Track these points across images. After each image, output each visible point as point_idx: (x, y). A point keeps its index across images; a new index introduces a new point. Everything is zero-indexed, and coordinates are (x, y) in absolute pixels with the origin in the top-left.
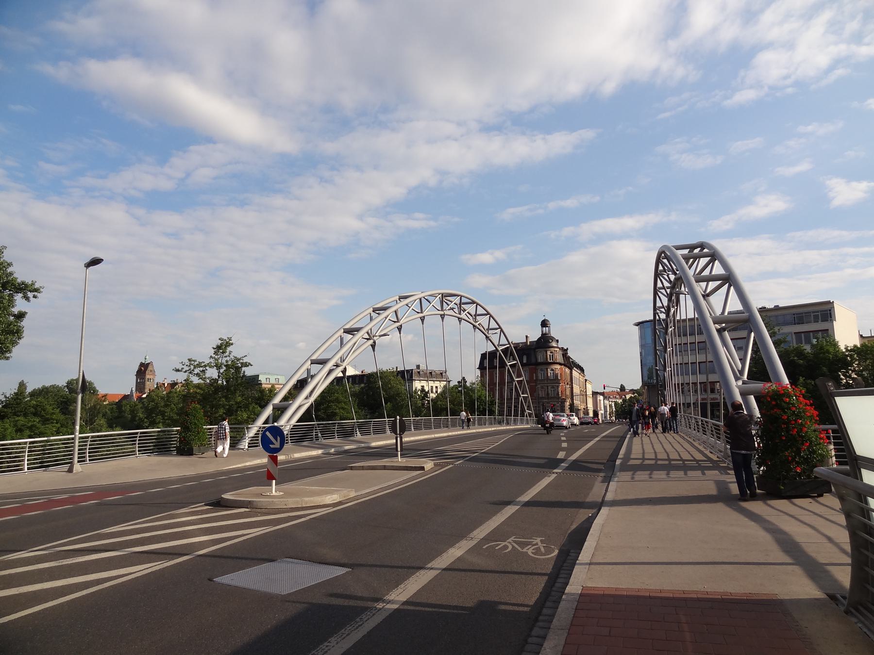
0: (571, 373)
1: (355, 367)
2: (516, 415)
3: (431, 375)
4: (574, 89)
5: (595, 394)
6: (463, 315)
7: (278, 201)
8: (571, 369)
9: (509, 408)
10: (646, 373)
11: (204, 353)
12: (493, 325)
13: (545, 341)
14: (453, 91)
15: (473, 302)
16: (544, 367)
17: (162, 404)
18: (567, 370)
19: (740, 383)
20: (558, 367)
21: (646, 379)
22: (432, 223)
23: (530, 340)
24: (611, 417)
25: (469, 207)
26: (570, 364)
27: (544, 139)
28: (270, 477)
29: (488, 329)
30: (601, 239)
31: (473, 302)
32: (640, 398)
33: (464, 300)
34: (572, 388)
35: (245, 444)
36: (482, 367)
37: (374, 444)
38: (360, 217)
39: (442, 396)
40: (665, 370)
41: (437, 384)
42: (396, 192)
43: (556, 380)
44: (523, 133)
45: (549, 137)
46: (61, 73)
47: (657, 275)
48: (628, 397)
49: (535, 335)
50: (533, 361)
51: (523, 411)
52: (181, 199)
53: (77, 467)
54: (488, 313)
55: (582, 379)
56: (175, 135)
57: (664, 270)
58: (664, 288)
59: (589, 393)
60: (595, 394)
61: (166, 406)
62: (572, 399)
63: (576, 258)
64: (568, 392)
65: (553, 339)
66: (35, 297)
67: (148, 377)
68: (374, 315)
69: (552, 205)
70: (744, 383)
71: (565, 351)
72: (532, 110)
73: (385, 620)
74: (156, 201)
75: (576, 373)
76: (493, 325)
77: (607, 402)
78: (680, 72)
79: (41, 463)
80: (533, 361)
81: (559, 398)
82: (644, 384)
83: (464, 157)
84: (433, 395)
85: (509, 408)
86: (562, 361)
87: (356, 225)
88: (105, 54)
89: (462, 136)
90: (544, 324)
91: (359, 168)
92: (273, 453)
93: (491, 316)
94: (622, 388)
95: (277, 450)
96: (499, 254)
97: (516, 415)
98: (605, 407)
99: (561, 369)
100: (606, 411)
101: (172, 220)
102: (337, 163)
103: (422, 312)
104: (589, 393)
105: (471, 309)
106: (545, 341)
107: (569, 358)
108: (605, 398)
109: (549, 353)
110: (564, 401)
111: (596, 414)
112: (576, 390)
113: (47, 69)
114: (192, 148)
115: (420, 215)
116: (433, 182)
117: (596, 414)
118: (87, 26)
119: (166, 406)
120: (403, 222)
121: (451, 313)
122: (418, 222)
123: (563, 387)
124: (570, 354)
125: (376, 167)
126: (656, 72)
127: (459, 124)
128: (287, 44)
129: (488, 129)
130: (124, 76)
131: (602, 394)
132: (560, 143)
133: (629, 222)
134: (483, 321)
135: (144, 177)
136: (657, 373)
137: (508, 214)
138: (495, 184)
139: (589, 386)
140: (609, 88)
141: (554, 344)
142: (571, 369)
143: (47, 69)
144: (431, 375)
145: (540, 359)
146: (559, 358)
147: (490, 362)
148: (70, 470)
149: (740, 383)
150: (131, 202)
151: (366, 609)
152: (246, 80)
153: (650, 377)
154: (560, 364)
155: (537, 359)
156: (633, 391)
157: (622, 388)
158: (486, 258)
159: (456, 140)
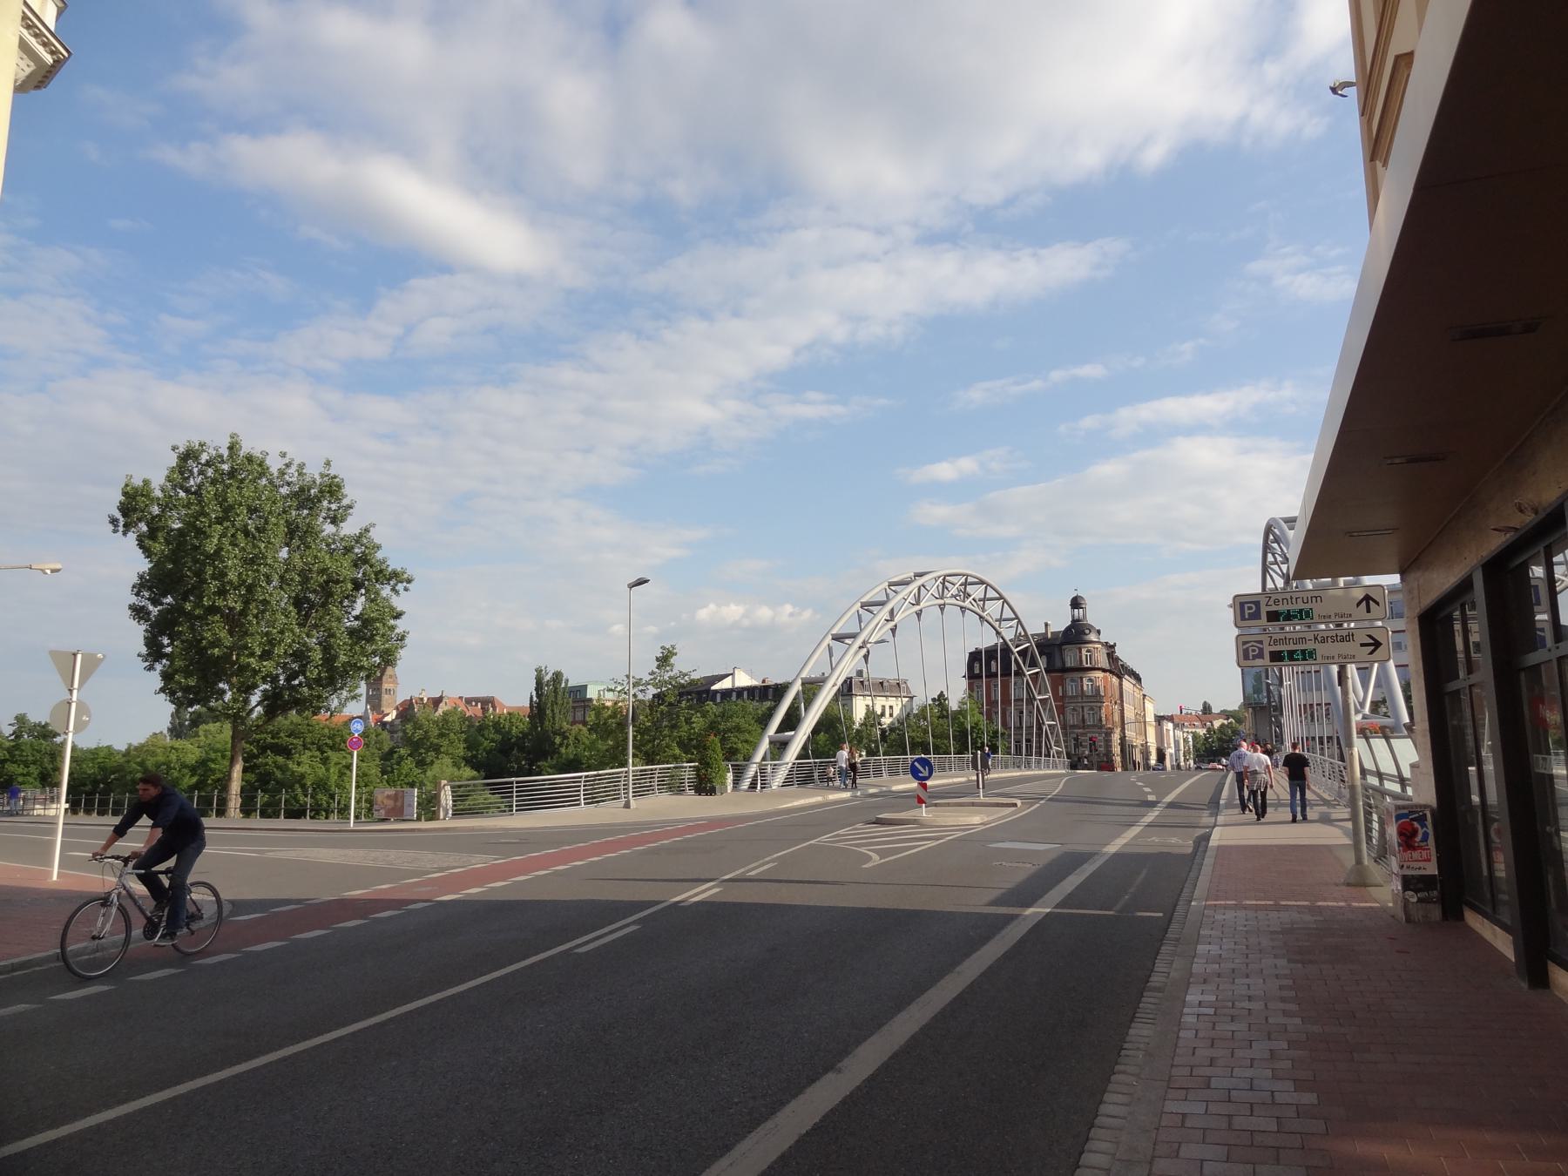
0: (1121, 685)
1: (751, 674)
2: (1029, 753)
3: (882, 687)
4: (1088, 159)
5: (1160, 719)
6: (967, 604)
7: (566, 374)
8: (1120, 677)
9: (1018, 742)
10: (1250, 682)
11: (644, 667)
12: (1008, 613)
13: (1076, 633)
14: (863, 167)
15: (982, 582)
16: (1076, 675)
17: (436, 732)
18: (1115, 680)
19: (1359, 717)
20: (1100, 674)
21: (1250, 690)
22: (839, 409)
23: (1052, 629)
24: (1186, 760)
25: (911, 384)
26: (1118, 669)
27: (1035, 255)
28: (921, 801)
29: (1000, 620)
30: (1154, 435)
31: (982, 582)
32: (1241, 728)
33: (970, 579)
34: (1122, 711)
35: (746, 784)
36: (972, 676)
37: (894, 788)
38: (711, 400)
39: (906, 719)
40: (1281, 684)
41: (892, 701)
42: (776, 355)
43: (1097, 697)
44: (997, 247)
45: (1043, 252)
46: (191, 160)
47: (1265, 570)
48: (1217, 724)
49: (1060, 623)
50: (1058, 664)
51: (1048, 749)
52: (399, 375)
53: (633, 803)
54: (1001, 597)
55: (1138, 696)
56: (387, 262)
57: (1276, 563)
58: (1276, 563)
59: (1150, 718)
60: (1160, 719)
61: (442, 735)
62: (1123, 729)
63: (1108, 470)
64: (1117, 718)
65: (1090, 628)
66: (406, 589)
67: (385, 686)
68: (866, 615)
69: (1057, 375)
70: (1364, 717)
71: (1110, 648)
72: (1010, 202)
73: (1030, 931)
74: (364, 378)
75: (1128, 684)
76: (1008, 613)
77: (1179, 733)
78: (1284, 124)
79: (592, 800)
80: (1058, 664)
81: (1101, 727)
82: (1248, 703)
83: (888, 291)
84: (886, 721)
85: (1018, 742)
86: (1107, 666)
87: (702, 412)
88: (256, 126)
89: (886, 253)
90: (1076, 603)
91: (705, 314)
92: (922, 780)
93: (1005, 601)
94: (1207, 709)
95: (926, 778)
96: (967, 464)
97: (1029, 753)
98: (1177, 743)
99: (1105, 678)
100: (1177, 750)
101: (384, 409)
102: (667, 308)
103: (918, 603)
104: (1150, 718)
105: (977, 592)
106: (1076, 633)
107: (1118, 659)
108: (1176, 726)
109: (1084, 652)
110: (1109, 733)
111: (1161, 756)
112: (1130, 713)
113: (169, 155)
114: (414, 282)
115: (812, 395)
116: (840, 334)
117: (1161, 756)
118: (232, 80)
119: (442, 735)
120: (791, 410)
121: (953, 601)
122: (813, 408)
123: (1108, 709)
124: (1118, 653)
125: (736, 314)
126: (1242, 121)
127: (880, 232)
128: (572, 100)
129: (932, 239)
130: (298, 161)
131: (1171, 719)
132: (1064, 265)
133: (1206, 405)
134: (993, 609)
135: (345, 338)
136: (1269, 691)
137: (977, 394)
138: (952, 342)
139: (1150, 707)
140: (1154, 156)
141: (1093, 637)
142: (1120, 677)
143: (169, 155)
144: (882, 687)
145: (1070, 662)
146: (1102, 660)
147: (982, 665)
148: (627, 806)
149: (1359, 717)
150: (317, 378)
151: (1017, 916)
152: (502, 163)
153: (1257, 690)
154: (1104, 670)
155: (1064, 663)
156: (1226, 714)
157: (1207, 709)
158: (944, 471)
159: (877, 261)
